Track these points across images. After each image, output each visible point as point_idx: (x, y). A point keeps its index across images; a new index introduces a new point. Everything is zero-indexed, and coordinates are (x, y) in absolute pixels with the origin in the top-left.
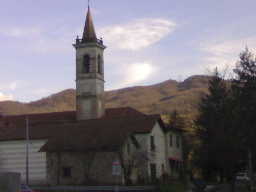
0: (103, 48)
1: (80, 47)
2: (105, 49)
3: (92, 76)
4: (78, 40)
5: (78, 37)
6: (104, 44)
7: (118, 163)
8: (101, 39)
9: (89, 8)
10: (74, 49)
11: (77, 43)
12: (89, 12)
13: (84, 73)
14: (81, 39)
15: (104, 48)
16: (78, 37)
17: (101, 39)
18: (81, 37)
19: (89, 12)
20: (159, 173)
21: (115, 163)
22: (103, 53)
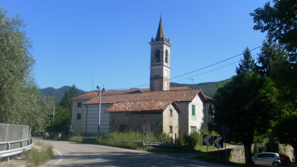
1: (154, 45)
3: (161, 64)
4: (152, 40)
5: (152, 37)
8: (169, 39)
9: (161, 18)
18: (155, 37)
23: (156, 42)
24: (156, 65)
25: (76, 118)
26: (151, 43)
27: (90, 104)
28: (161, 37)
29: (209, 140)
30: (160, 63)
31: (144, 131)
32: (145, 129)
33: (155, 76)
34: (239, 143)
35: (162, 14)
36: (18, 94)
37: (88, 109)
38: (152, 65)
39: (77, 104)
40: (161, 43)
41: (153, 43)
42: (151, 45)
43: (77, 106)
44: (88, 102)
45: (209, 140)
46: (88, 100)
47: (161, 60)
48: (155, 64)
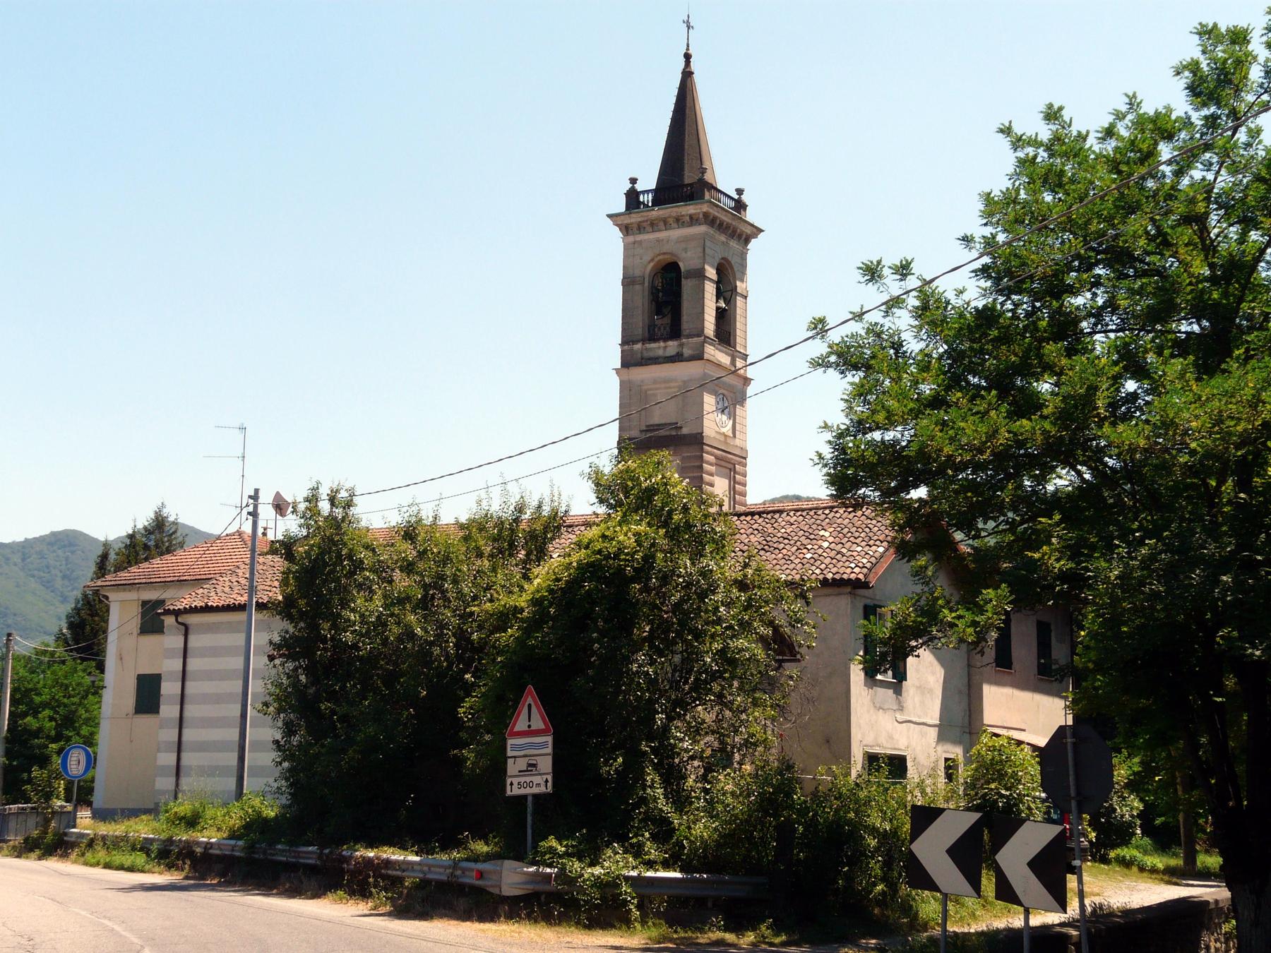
0: (743, 234)
1: (640, 228)
2: (755, 236)
3: (687, 352)
4: (633, 197)
5: (633, 181)
6: (751, 215)
7: (538, 723)
8: (740, 192)
9: (688, 57)
10: (616, 235)
11: (628, 207)
12: (687, 75)
13: (652, 338)
14: (647, 192)
15: (748, 230)
16: (633, 181)
17: (740, 192)
18: (648, 181)
19: (687, 75)
20: (834, 493)
21: (521, 725)
22: (743, 256)
23: (657, 212)
24: (655, 361)
25: (130, 700)
26: (627, 220)
27: (207, 609)
28: (689, 177)
29: (952, 852)
30: (682, 345)
31: (515, 781)
32: (522, 764)
33: (651, 428)
34: (275, 891)
35: (691, 31)
36: (397, 575)
37: (194, 641)
38: (628, 362)
39: (135, 612)
40: (691, 217)
41: (635, 218)
42: (626, 230)
43: (136, 630)
44: (188, 599)
45: (952, 852)
46: (199, 582)
47: (687, 324)
48: (651, 354)
